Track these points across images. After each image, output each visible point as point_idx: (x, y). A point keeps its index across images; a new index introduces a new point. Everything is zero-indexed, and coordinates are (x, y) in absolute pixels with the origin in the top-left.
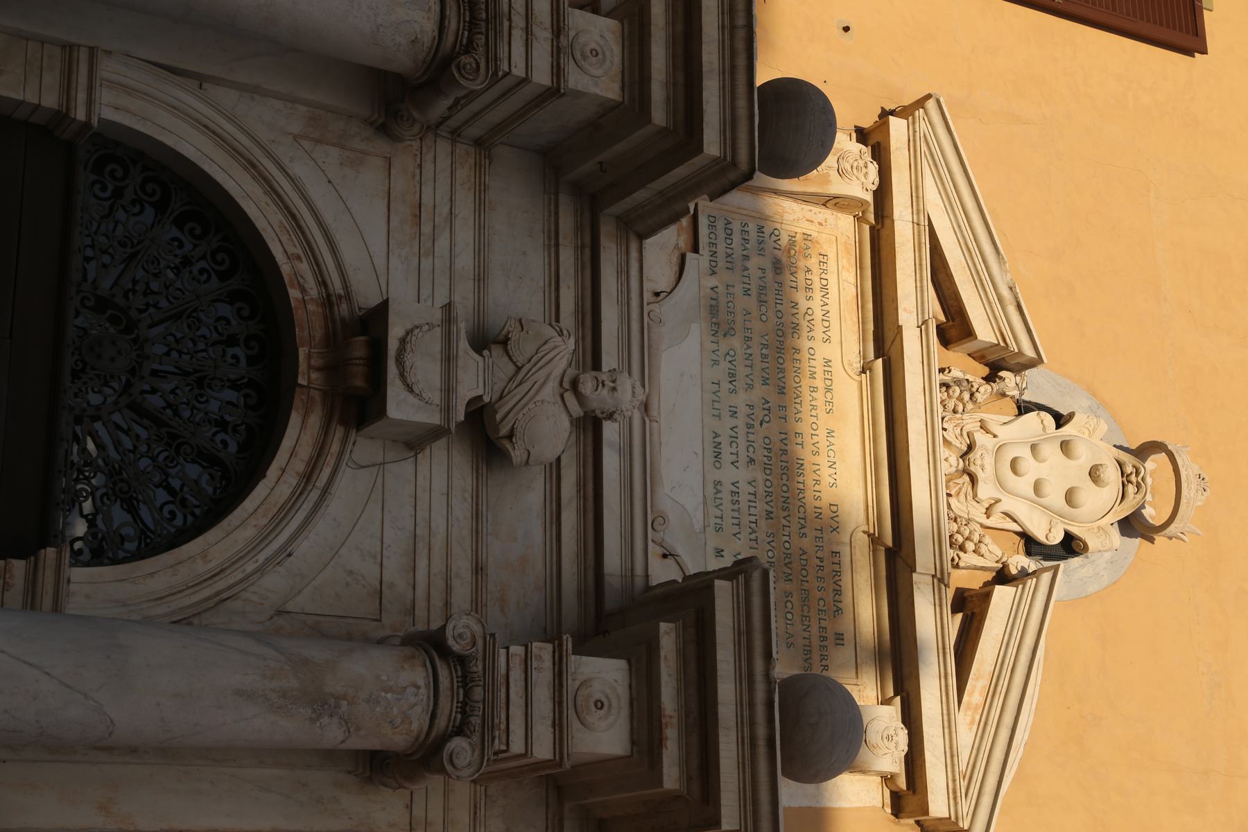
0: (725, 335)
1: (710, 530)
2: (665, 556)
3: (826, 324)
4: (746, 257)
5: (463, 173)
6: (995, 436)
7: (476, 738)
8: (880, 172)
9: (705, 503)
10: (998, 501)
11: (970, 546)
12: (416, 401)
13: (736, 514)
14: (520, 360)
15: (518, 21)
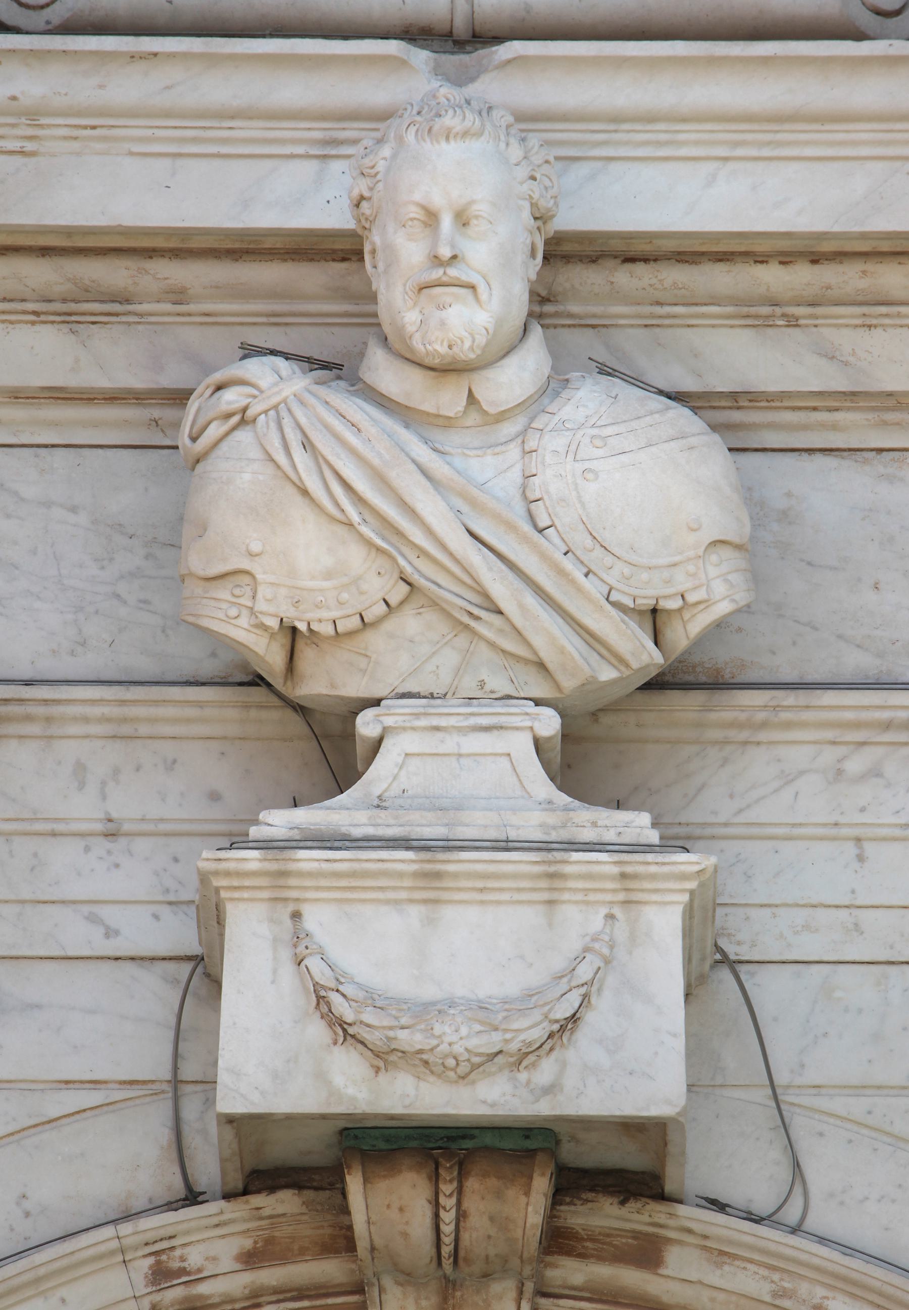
14: (378, 586)
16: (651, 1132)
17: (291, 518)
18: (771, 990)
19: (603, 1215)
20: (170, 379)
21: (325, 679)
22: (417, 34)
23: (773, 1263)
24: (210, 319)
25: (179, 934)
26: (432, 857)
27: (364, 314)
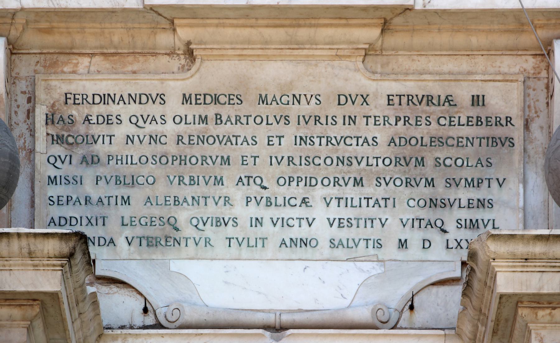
0: (177, 229)
1: (382, 254)
2: (412, 308)
4: (88, 200)
9: (354, 260)
13: (362, 223)
22: (267, 327)
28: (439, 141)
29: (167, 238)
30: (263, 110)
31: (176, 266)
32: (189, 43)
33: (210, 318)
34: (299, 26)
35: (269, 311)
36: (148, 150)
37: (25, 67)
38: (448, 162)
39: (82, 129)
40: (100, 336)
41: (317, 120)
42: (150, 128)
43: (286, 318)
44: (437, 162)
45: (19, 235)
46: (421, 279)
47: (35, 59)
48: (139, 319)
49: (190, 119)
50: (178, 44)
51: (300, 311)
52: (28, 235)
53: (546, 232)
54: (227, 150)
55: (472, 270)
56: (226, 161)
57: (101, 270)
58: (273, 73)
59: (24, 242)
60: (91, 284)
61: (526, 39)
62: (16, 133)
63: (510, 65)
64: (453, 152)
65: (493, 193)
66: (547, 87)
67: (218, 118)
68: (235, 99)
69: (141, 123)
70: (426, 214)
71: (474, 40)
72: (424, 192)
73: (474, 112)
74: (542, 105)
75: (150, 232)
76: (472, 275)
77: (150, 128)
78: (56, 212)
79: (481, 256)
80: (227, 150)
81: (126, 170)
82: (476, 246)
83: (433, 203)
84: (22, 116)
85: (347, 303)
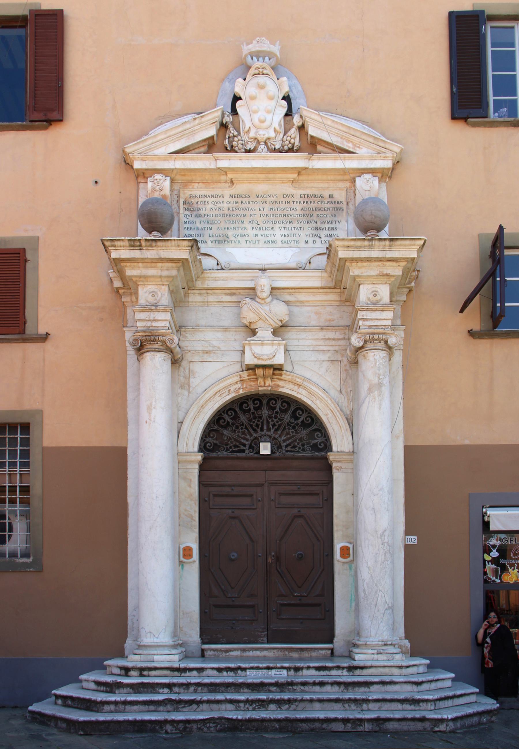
0: (228, 238)
1: (299, 245)
2: (310, 263)
3: (216, 196)
4: (197, 229)
5: (189, 336)
6: (250, 128)
7: (388, 336)
8: (158, 173)
9: (290, 247)
10: (275, 129)
11: (292, 141)
12: (277, 354)
13: (292, 235)
14: (257, 318)
15: (149, 324)
16: (281, 365)
17: (250, 312)
18: (291, 353)
19: (277, 372)
20: (239, 300)
21: (252, 327)
22: (260, 270)
23: (291, 376)
24: (242, 295)
25: (241, 349)
26: (262, 342)
27: (256, 294)
28: (318, 209)
29: (225, 241)
30: (258, 200)
31: (228, 250)
32: (232, 179)
33: (240, 267)
34: (270, 173)
35: (260, 264)
36: (218, 212)
37: (176, 187)
38: (321, 216)
39: (196, 206)
40: (202, 273)
41: (276, 203)
42: (219, 205)
43: (266, 267)
44: (318, 216)
45: (174, 240)
46: (313, 253)
47: (179, 184)
48: (216, 267)
49: (232, 203)
50: (228, 179)
51: (271, 264)
52: (177, 240)
53: (355, 238)
54: (245, 212)
55: (330, 250)
56: (245, 216)
57: (202, 251)
58: (261, 188)
59: (176, 242)
60: (199, 256)
61: (347, 177)
62: (173, 207)
63: (341, 185)
64: (323, 212)
65: (337, 225)
66: (354, 192)
67: (242, 202)
68: (248, 196)
69: (215, 204)
70: (314, 232)
71: (329, 178)
72: (313, 225)
73: (330, 200)
74: (352, 197)
75: (219, 239)
76: (330, 252)
77: (219, 205)
78: (187, 232)
79: (333, 246)
80: (245, 212)
81: (211, 219)
82: (331, 243)
83: (317, 229)
84: (175, 202)
85: (287, 261)
